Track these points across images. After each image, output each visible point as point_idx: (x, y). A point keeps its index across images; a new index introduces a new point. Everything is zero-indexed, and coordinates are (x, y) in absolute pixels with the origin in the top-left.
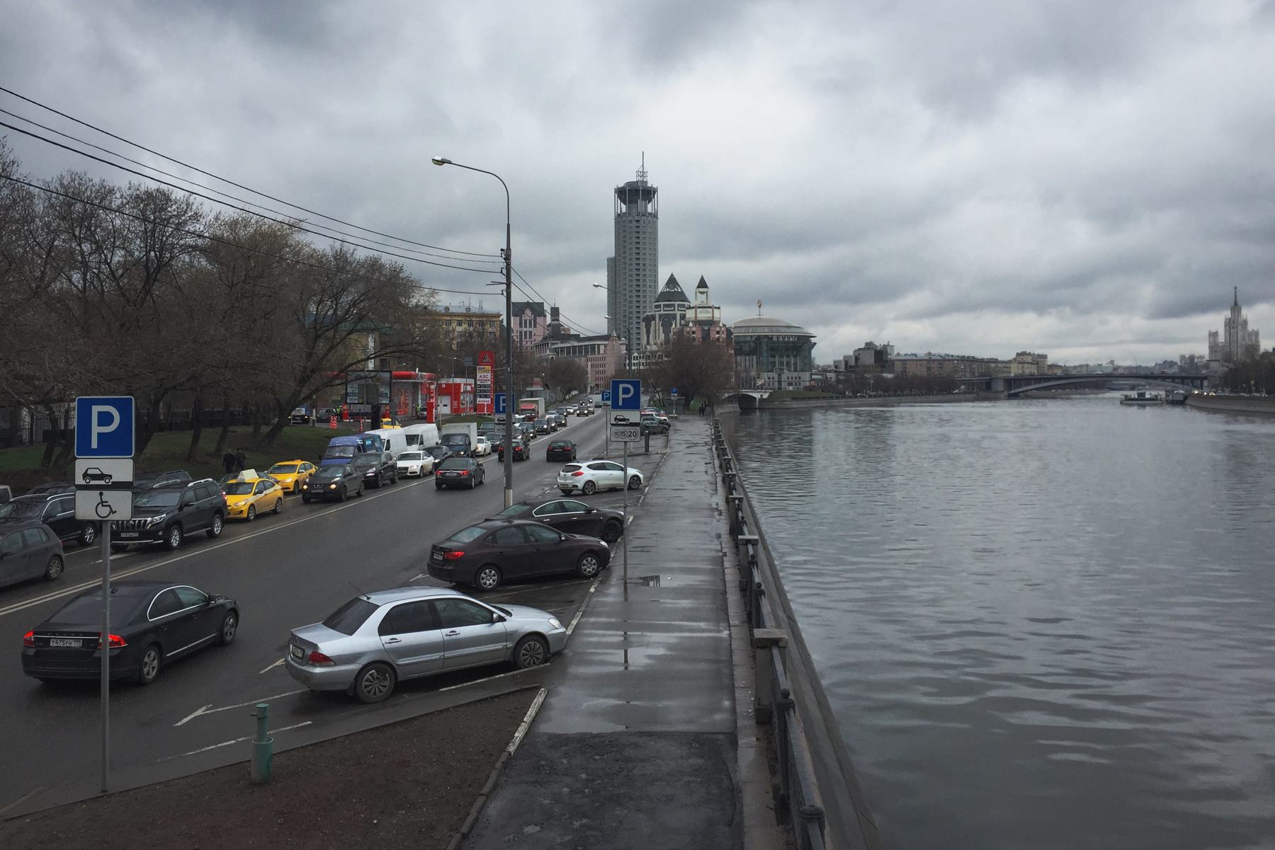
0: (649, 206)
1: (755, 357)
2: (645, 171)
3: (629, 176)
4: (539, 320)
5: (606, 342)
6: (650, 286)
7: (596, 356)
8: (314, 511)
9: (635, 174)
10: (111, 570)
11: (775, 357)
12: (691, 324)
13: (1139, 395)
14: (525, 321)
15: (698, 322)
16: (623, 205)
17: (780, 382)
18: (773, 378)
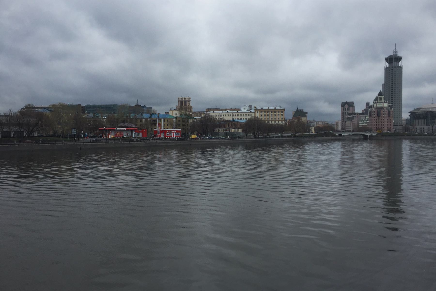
1: (426, 120)
2: (396, 50)
4: (351, 108)
5: (355, 116)
6: (397, 94)
7: (354, 120)
10: (240, 111)
12: (385, 109)
14: (346, 108)
15: (377, 108)
17: (432, 129)
18: (430, 128)
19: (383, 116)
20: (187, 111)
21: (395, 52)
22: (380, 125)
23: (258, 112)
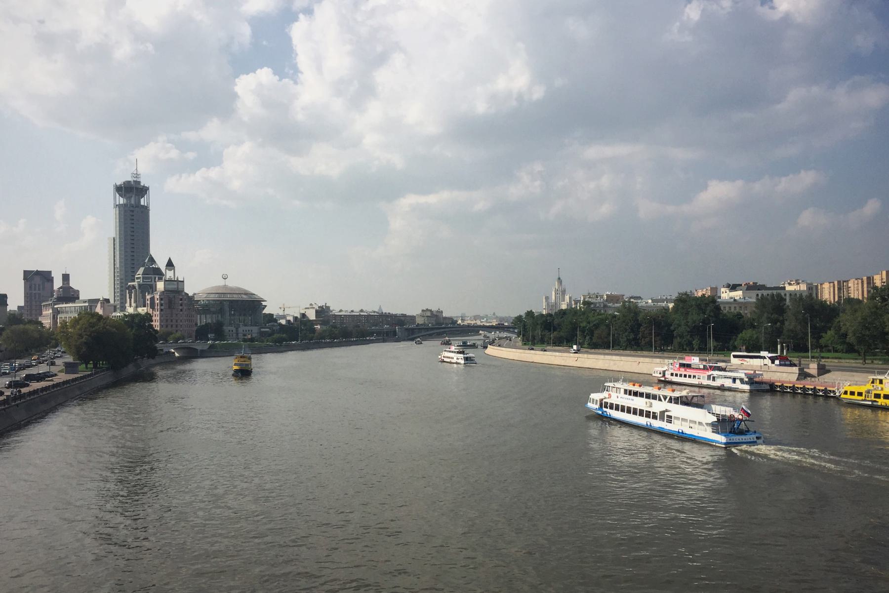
0: (142, 200)
18: (232, 331)
19: (181, 308)
22: (174, 326)
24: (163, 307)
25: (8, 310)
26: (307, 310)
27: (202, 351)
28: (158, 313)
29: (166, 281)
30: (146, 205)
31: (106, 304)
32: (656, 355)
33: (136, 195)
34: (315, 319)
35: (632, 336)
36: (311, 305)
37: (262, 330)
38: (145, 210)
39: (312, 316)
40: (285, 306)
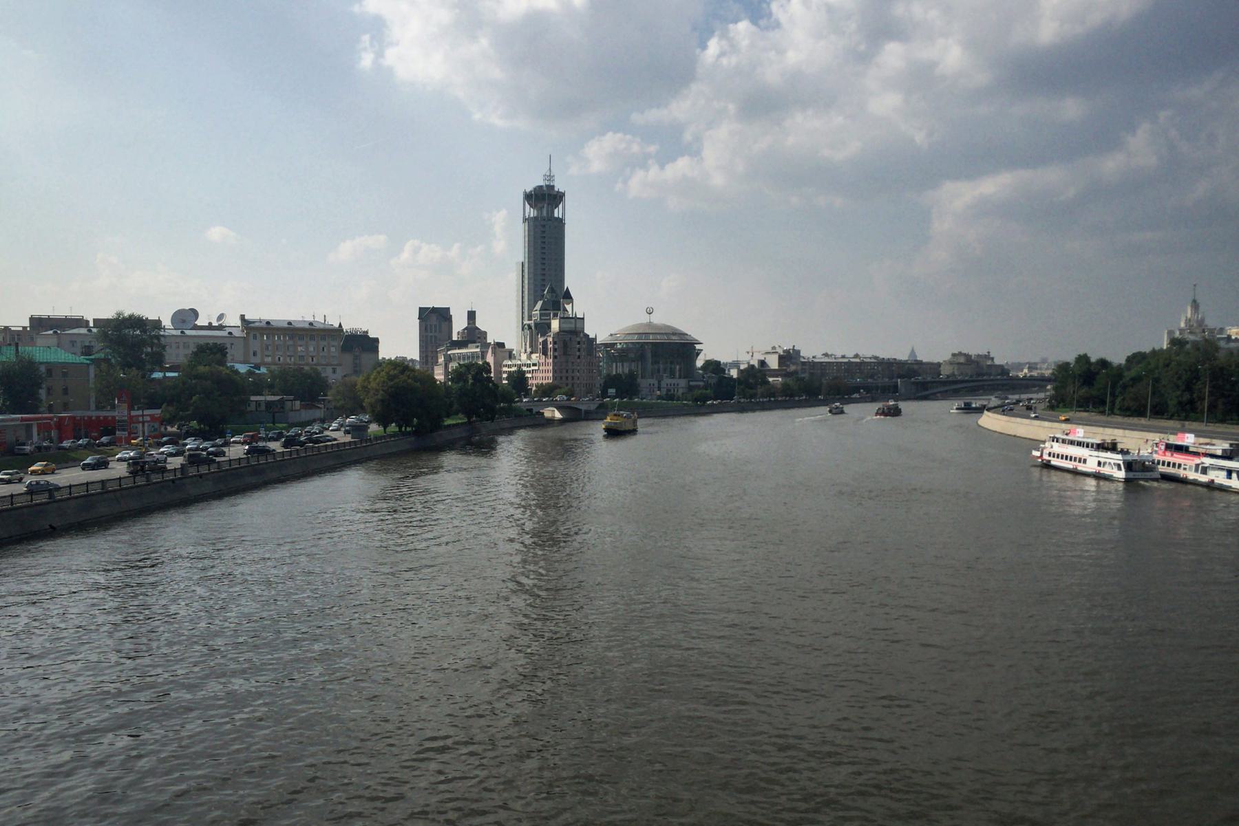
0: (556, 211)
3: (535, 181)
8: (652, 425)
9: (542, 178)
11: (659, 363)
13: (965, 404)
16: (532, 210)
19: (578, 354)
20: (900, 376)
21: (550, 177)
23: (255, 337)
24: (556, 354)
25: (380, 358)
26: (766, 356)
27: (587, 412)
28: (551, 360)
29: (561, 318)
30: (560, 217)
31: (498, 350)
32: (1209, 428)
33: (548, 204)
34: (777, 368)
35: (1186, 397)
36: (774, 348)
37: (691, 383)
38: (560, 223)
39: (773, 363)
40: (754, 350)
